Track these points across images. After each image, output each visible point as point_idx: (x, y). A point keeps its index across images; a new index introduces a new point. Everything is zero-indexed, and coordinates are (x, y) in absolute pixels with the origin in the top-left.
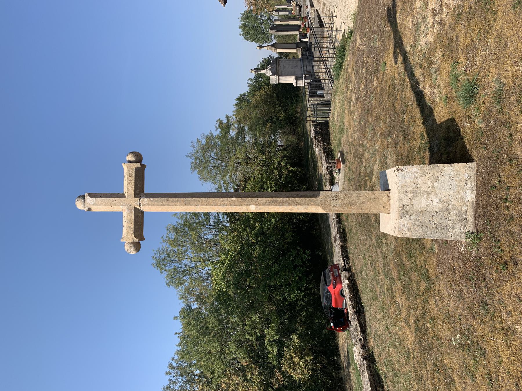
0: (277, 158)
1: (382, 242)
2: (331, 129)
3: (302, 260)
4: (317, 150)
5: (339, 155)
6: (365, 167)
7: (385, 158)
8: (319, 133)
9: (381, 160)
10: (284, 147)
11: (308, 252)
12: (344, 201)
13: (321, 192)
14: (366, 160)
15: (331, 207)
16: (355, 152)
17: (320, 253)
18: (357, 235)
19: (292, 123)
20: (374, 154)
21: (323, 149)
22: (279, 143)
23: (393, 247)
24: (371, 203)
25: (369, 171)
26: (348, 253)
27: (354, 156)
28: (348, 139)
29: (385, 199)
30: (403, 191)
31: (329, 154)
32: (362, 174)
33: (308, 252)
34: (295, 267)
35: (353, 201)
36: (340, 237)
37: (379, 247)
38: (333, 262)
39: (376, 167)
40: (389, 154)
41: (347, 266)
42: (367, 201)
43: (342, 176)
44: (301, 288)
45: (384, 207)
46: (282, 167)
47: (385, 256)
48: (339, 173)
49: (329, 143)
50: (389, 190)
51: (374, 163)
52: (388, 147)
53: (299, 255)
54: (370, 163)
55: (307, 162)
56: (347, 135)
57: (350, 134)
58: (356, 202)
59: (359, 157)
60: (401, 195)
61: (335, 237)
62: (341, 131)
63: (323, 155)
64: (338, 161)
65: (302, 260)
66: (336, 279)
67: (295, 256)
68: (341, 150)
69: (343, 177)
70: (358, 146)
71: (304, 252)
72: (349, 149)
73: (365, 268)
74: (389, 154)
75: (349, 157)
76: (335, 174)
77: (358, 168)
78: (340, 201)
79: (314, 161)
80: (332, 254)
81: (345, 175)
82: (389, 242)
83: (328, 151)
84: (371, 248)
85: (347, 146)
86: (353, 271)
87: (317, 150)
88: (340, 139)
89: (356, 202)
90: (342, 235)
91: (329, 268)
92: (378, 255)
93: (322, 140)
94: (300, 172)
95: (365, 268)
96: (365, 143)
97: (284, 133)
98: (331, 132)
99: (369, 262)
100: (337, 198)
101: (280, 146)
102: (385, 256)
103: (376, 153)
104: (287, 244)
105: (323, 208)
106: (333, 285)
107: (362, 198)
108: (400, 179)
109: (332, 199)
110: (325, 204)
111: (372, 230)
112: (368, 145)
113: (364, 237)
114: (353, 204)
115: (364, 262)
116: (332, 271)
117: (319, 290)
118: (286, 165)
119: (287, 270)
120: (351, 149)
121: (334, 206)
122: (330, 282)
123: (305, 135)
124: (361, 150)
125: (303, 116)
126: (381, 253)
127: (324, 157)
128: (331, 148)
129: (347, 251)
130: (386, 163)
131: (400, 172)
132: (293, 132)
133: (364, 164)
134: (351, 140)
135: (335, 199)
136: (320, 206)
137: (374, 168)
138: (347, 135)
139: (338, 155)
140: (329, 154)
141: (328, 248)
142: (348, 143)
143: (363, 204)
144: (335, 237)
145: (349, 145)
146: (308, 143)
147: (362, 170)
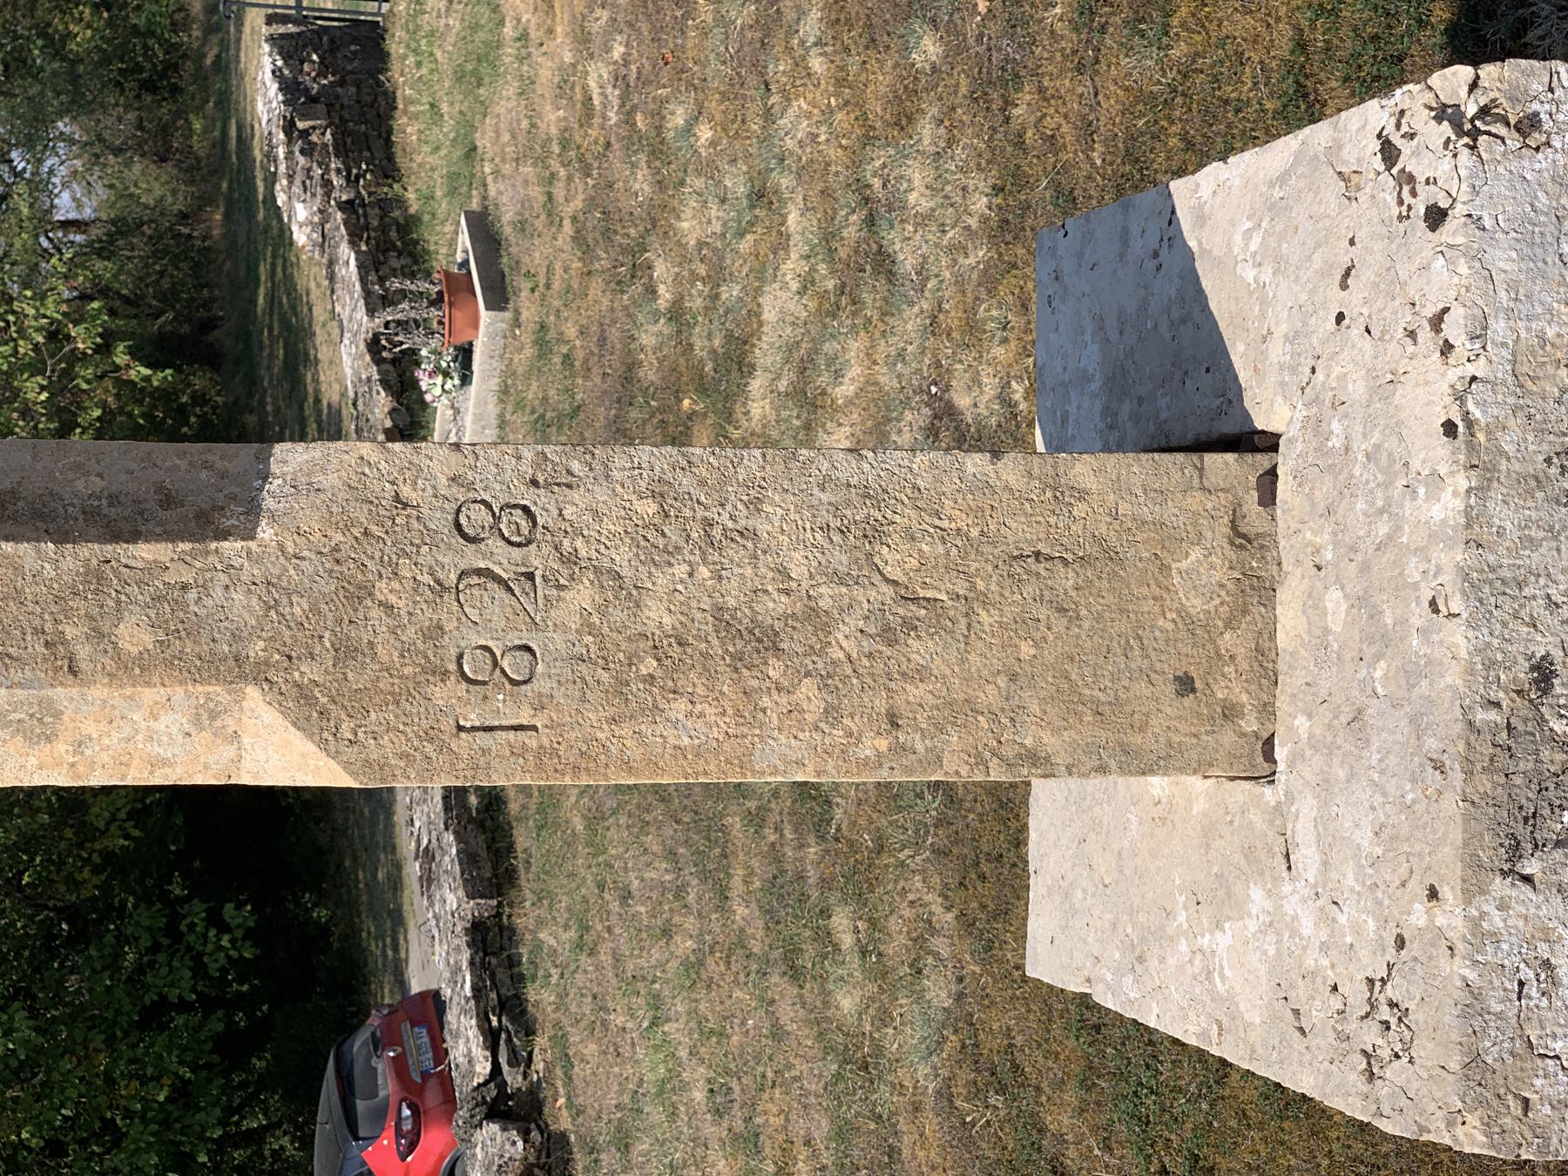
0: (41, 297)
1: (825, 937)
2: (405, 74)
3: (199, 968)
4: (301, 217)
5: (464, 240)
6: (676, 313)
7: (871, 222)
8: (314, 100)
9: (829, 237)
10: (95, 232)
11: (239, 915)
12: (634, 597)
13: (289, 458)
14: (685, 260)
15: (445, 693)
16: (591, 203)
17: (321, 914)
18: (597, 848)
19: (149, 86)
20: (761, 195)
21: (342, 206)
22: (64, 206)
23: (939, 992)
24: (1025, 624)
25: (705, 342)
26: (519, 980)
27: (578, 238)
28: (533, 114)
29: (1202, 573)
30: (1538, 450)
31: (389, 244)
32: (649, 373)
33: (239, 915)
34: (154, 1017)
35: (774, 606)
36: (468, 859)
37: (795, 974)
38: (401, 982)
39: (781, 306)
40: (917, 175)
41: (514, 1079)
42: (972, 601)
43: (481, 402)
44: (192, 1156)
45: (1186, 685)
46: (77, 358)
47: (861, 1062)
48: (466, 380)
49: (389, 170)
50: (1254, 442)
51: (762, 274)
52: (904, 121)
53: (177, 937)
54: (717, 277)
55: (245, 335)
56: (527, 87)
57: (546, 73)
58: (818, 620)
59: (619, 244)
60: (1504, 515)
61: (427, 856)
62: (476, 70)
63: (346, 252)
64: (458, 285)
65: (199, 968)
66: (420, 1090)
67: (155, 948)
68: (475, 205)
69: (493, 410)
70: (616, 158)
71: (215, 919)
72: (536, 192)
73: (655, 1113)
74: (917, 175)
75: (543, 254)
76: (431, 386)
77: (614, 334)
78: (582, 595)
79: (286, 326)
80: (397, 919)
81: (505, 391)
82: (896, 944)
83: (384, 229)
84: (714, 967)
85: (527, 170)
86: (561, 1118)
87: (302, 212)
88: (467, 127)
89: (818, 620)
90: (479, 841)
91: (374, 1020)
92: (778, 1033)
93: (341, 150)
94: (199, 399)
95: (655, 1113)
96: (678, 117)
97: (98, 149)
98: (405, 92)
99: (697, 1079)
100: (538, 559)
101: (67, 225)
102: (861, 1062)
103: (786, 182)
104: (96, 871)
105: (309, 712)
106: (399, 1133)
107: (894, 560)
108: (1503, 259)
109: (453, 559)
110: (345, 652)
111: (735, 822)
112: (705, 133)
113: (660, 872)
114: (768, 641)
115: (651, 1070)
116: (391, 1044)
117: (307, 1143)
118: (104, 349)
119: (98, 1040)
120: (559, 192)
121: (491, 675)
122: (380, 1114)
123: (227, 174)
124: (642, 184)
125: (224, 45)
126: (821, 1021)
127: (349, 267)
128: (401, 202)
129: (513, 962)
130: (883, 263)
131: (1499, 147)
132: (159, 145)
133: (665, 294)
134: (552, 118)
135: (502, 559)
136: (259, 674)
137: (755, 314)
138: (527, 87)
139: (453, 244)
140: (389, 244)
141: (372, 883)
142: (533, 149)
143: (918, 649)
144: (427, 856)
145: (541, 161)
146: (251, 216)
147: (647, 339)
